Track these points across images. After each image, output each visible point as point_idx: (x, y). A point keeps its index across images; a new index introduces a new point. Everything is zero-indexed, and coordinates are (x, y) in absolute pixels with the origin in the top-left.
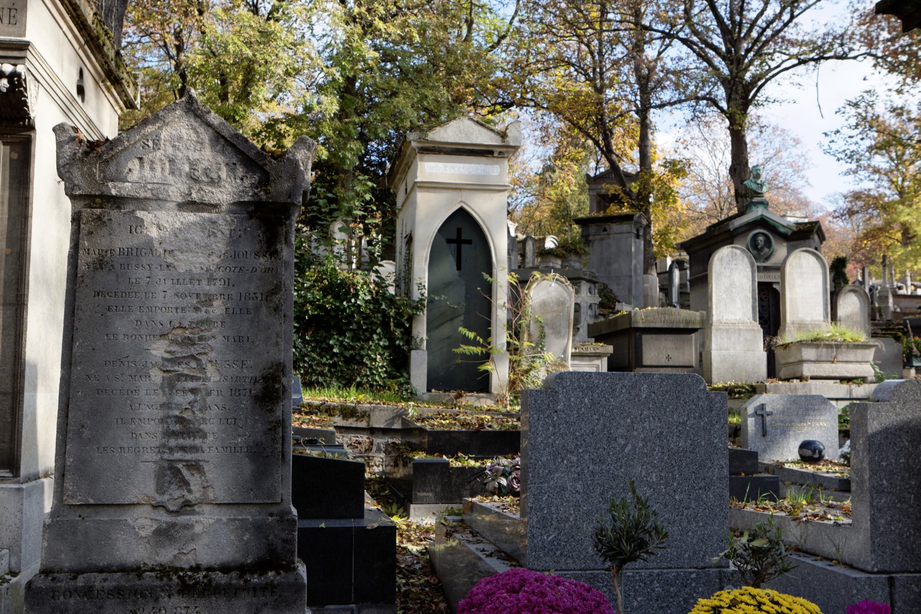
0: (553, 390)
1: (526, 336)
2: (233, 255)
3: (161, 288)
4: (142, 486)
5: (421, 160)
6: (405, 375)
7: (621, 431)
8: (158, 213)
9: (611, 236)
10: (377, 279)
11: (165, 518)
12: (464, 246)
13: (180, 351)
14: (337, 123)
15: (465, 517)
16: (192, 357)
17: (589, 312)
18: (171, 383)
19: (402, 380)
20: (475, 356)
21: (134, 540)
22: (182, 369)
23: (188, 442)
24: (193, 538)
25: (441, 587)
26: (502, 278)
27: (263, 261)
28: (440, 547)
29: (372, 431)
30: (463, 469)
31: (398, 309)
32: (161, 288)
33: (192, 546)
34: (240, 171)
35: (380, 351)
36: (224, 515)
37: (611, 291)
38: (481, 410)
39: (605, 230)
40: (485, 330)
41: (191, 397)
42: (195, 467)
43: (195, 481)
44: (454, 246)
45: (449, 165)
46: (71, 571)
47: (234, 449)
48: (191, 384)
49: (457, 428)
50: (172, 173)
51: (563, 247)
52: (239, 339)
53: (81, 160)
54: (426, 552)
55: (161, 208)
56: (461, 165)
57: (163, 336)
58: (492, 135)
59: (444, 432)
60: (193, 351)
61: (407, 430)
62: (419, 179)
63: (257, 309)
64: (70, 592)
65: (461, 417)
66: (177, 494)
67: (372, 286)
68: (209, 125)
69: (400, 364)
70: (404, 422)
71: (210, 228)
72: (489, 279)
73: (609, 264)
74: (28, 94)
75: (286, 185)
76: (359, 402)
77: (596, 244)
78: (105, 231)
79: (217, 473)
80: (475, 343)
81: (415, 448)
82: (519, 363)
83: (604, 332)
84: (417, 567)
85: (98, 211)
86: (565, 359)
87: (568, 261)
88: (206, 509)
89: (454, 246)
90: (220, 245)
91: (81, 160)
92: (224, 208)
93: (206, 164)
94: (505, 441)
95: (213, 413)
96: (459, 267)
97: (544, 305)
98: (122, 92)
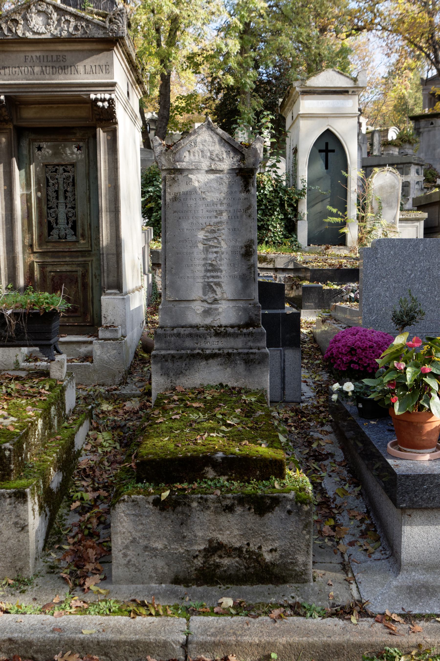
0: (375, 248)
1: (370, 208)
2: (230, 193)
3: (201, 208)
4: (197, 292)
5: (303, 99)
6: (294, 236)
7: (409, 267)
8: (198, 175)
9: (437, 128)
10: (276, 177)
11: (207, 306)
12: (330, 154)
13: (210, 236)
14: (240, 58)
15: (332, 313)
16: (215, 238)
17: (417, 187)
18: (207, 249)
19: (292, 239)
20: (337, 224)
21: (195, 315)
22: (211, 243)
23: (215, 274)
24: (219, 314)
25: (320, 349)
26: (355, 173)
27: (243, 195)
28: (318, 331)
29: (276, 270)
30: (330, 290)
31: (289, 195)
32: (201, 208)
33: (218, 317)
34: (232, 154)
35: (279, 221)
36: (231, 304)
37: (435, 169)
38: (341, 257)
39: (432, 124)
40: (343, 207)
41: (215, 255)
42: (218, 284)
43: (218, 290)
44: (323, 154)
45: (320, 101)
46: (171, 327)
47: (234, 277)
48: (215, 250)
49: (327, 267)
50: (203, 157)
51: (400, 139)
52: (234, 230)
53: (165, 153)
54: (312, 332)
55: (199, 173)
56: (328, 101)
57: (203, 229)
58: (348, 80)
59: (319, 270)
60: (215, 235)
61: (297, 269)
62: (301, 112)
63: (242, 216)
64: (171, 335)
65: (329, 261)
66: (211, 296)
67: (273, 182)
68: (217, 134)
69: (291, 228)
70: (295, 264)
71: (220, 181)
72: (346, 175)
73: (434, 149)
74: (116, 108)
75: (252, 160)
76: (268, 253)
77: (425, 134)
78: (176, 184)
79: (227, 288)
80: (337, 216)
81: (302, 279)
82: (364, 227)
83: (423, 203)
84: (307, 340)
85: (173, 176)
86: (394, 223)
87: (404, 149)
88: (223, 302)
89: (323, 154)
90: (225, 189)
91: (165, 153)
92: (225, 172)
93: (217, 152)
94: (352, 275)
95: (225, 261)
96: (327, 168)
97: (382, 188)
98: (143, 88)
